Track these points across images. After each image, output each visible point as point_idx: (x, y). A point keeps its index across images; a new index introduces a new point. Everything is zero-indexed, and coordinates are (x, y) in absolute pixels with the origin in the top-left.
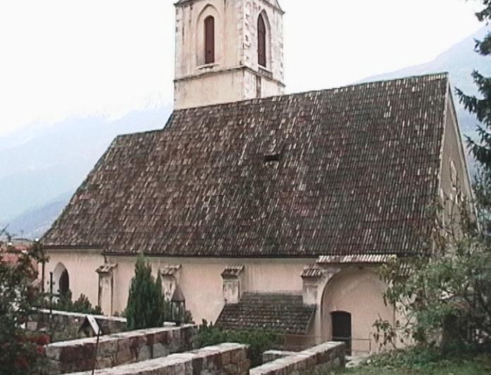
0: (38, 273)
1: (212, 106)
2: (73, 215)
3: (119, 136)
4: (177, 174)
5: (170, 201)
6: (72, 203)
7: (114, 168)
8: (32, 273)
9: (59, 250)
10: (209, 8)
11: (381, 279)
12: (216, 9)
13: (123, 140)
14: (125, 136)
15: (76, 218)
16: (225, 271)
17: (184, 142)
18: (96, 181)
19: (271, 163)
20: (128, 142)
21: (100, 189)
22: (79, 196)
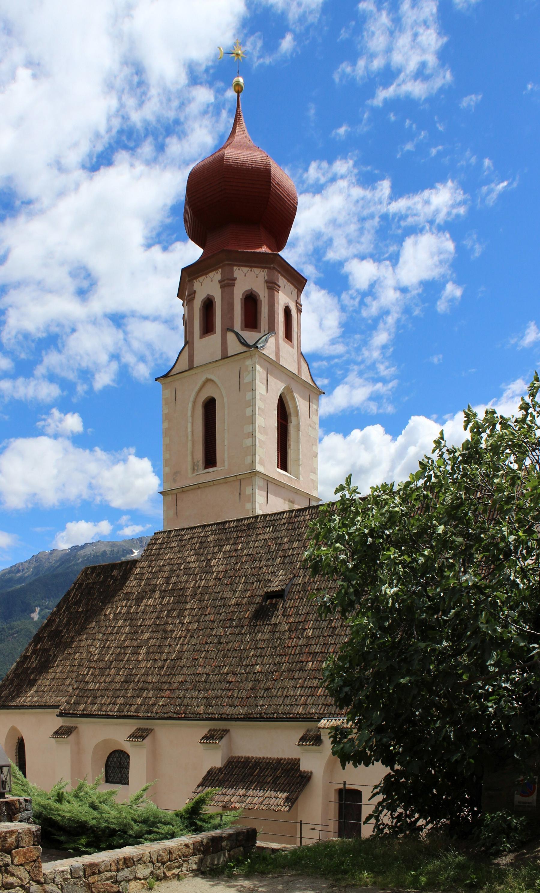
0: (92, 865)
1: (204, 526)
2: (28, 668)
3: (87, 568)
4: (154, 615)
5: (143, 650)
6: (28, 654)
7: (80, 610)
8: (346, 689)
9: (312, 389)
10: (209, 385)
11: (329, 733)
12: (220, 390)
13: (92, 572)
14: (95, 567)
15: (32, 673)
16: (139, 729)
17: (166, 574)
18: (58, 626)
19: (274, 601)
20: (98, 575)
21: (63, 636)
22: (36, 645)
